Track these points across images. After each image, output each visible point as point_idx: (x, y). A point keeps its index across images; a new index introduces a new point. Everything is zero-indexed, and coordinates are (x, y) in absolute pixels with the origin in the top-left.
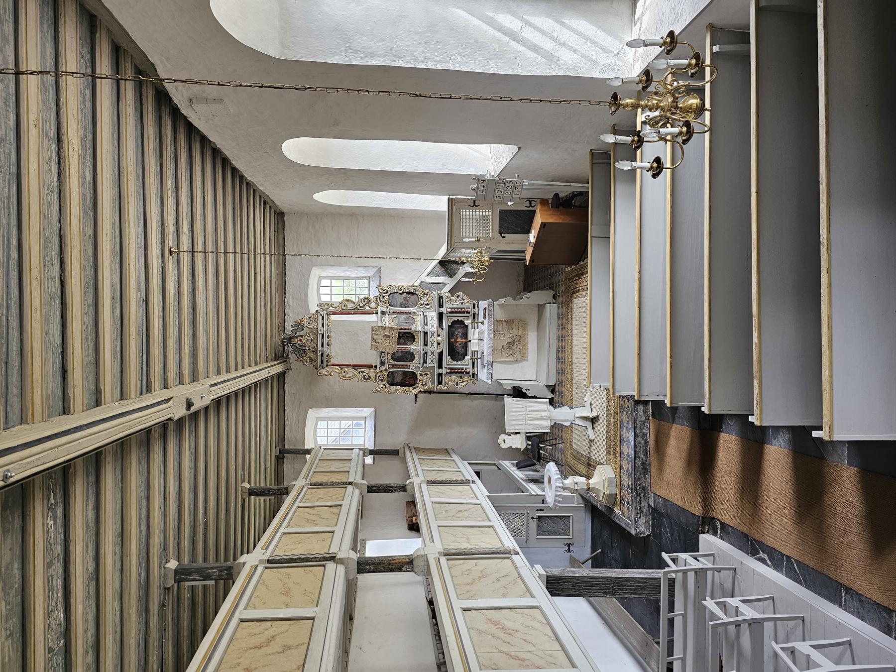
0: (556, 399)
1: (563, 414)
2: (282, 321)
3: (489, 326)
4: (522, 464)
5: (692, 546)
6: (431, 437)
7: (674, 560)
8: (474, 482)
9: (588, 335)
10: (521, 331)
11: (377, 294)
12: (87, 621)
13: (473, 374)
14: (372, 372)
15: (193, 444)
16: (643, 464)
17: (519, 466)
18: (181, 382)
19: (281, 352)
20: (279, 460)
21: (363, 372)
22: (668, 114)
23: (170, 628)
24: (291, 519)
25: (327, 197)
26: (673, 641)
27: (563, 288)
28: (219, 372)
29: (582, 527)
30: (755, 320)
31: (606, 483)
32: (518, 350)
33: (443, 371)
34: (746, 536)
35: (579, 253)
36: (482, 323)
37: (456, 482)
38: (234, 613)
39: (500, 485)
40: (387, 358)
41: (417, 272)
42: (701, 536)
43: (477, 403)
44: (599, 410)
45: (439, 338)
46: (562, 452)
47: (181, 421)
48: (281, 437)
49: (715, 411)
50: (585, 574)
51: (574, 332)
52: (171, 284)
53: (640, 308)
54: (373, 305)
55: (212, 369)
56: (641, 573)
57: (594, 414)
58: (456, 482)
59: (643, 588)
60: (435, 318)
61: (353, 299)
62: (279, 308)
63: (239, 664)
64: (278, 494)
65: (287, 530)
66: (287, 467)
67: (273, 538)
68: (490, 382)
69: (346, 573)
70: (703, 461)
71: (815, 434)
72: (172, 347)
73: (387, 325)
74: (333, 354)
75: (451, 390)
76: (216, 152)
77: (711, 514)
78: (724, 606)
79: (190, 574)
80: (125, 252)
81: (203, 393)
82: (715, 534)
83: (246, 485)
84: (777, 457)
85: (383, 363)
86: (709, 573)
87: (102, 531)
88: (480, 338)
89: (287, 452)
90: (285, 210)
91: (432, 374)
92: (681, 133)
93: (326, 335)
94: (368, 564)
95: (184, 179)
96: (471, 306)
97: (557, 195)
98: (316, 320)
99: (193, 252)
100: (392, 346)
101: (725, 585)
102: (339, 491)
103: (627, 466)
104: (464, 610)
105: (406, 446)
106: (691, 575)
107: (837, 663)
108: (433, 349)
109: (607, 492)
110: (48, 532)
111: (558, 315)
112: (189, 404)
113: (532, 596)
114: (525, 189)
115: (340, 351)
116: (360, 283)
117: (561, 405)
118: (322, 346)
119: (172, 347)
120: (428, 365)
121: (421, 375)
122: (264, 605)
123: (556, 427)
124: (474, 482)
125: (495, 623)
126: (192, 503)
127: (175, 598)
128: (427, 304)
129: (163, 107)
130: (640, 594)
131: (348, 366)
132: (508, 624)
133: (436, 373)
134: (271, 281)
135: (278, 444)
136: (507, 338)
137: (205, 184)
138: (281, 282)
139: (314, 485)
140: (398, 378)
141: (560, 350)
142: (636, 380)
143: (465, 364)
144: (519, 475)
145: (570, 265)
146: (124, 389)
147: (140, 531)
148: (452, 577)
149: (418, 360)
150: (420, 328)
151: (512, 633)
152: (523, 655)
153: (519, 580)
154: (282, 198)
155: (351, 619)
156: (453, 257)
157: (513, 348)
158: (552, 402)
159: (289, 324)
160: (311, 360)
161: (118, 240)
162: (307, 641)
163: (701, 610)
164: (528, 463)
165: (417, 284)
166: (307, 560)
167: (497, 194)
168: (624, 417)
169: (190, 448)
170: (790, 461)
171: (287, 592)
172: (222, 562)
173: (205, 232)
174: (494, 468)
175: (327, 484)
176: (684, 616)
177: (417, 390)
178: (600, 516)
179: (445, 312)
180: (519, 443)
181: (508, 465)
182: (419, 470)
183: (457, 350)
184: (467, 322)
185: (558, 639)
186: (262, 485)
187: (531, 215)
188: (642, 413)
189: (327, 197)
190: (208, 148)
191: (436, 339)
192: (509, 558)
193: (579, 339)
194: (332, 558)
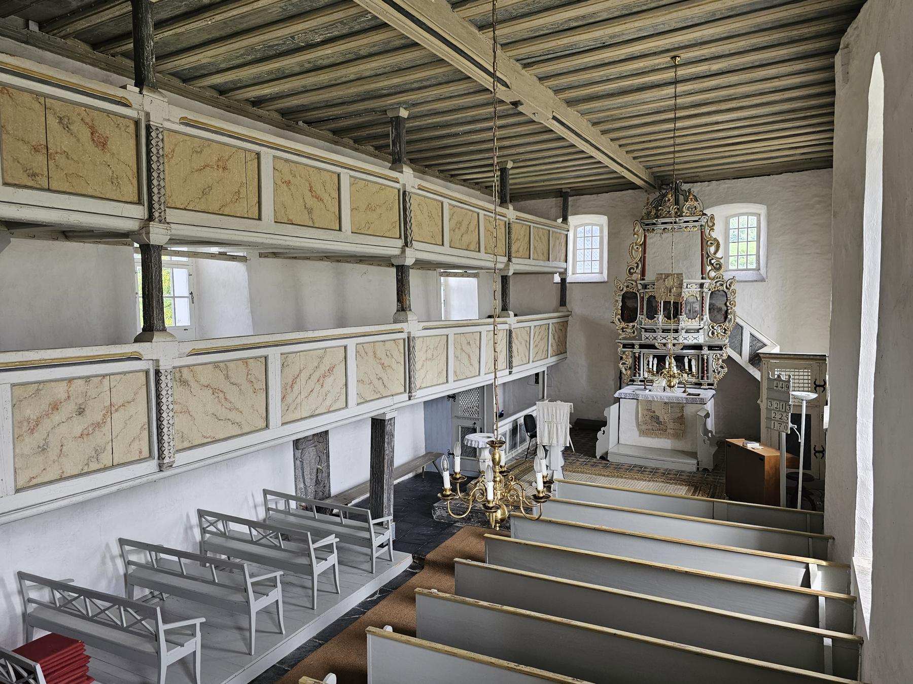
2: (702, 179)
3: (677, 398)
5: (399, 545)
10: (672, 432)
11: (726, 278)
12: (328, 58)
13: (633, 381)
21: (637, 267)
30: (498, 606)
33: (637, 350)
36: (684, 392)
53: (594, 529)
54: (713, 274)
56: (389, 500)
59: (376, 499)
60: (695, 341)
61: (719, 255)
62: (717, 174)
63: (295, 176)
69: (395, 256)
79: (396, 129)
80: (636, 17)
82: (411, 567)
83: (510, 165)
85: (645, 286)
87: (389, 55)
89: (564, 199)
93: (676, 226)
95: (774, 54)
96: (710, 381)
98: (693, 214)
108: (659, 338)
110: (362, 16)
120: (643, 334)
125: (331, 370)
128: (713, 333)
129: (845, 17)
131: (644, 251)
132: (329, 381)
138: (747, 173)
139: (509, 227)
140: (630, 304)
146: (510, 45)
147: (412, 83)
149: (647, 323)
150: (682, 324)
151: (321, 380)
152: (296, 387)
153: (379, 396)
157: (652, 421)
160: (648, 214)
161: (645, 8)
165: (738, 320)
179: (703, 352)
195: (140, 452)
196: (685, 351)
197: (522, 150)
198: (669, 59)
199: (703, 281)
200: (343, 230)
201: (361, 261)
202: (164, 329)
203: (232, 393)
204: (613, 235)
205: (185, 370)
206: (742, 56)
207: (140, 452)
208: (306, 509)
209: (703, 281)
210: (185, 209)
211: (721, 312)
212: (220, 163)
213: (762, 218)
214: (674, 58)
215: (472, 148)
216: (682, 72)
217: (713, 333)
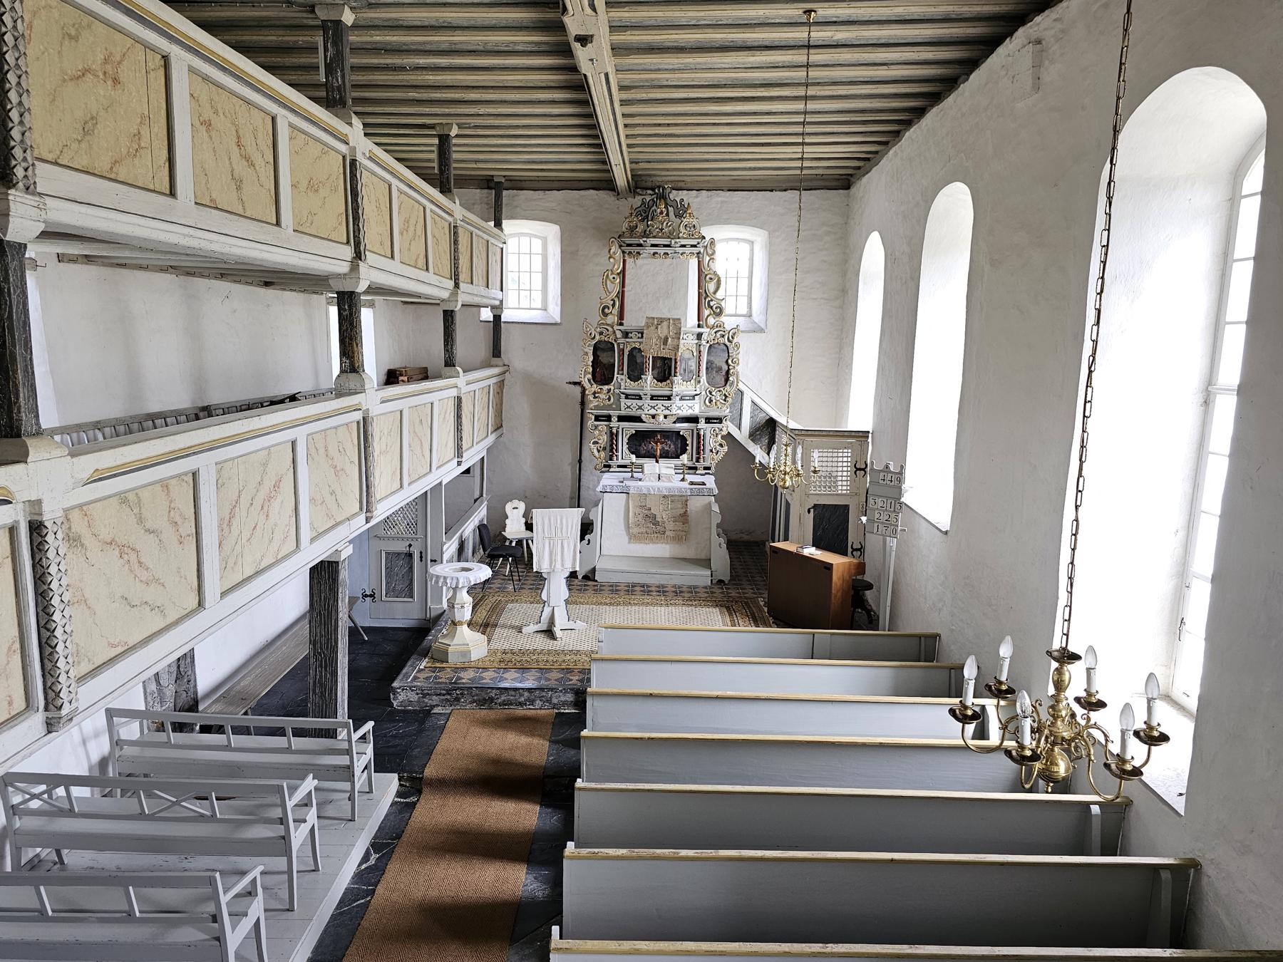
0: (576, 582)
1: (557, 590)
2: (688, 186)
3: (680, 489)
4: (484, 532)
5: (382, 763)
6: (519, 407)
7: (363, 738)
8: (459, 463)
9: (667, 625)
11: (728, 327)
13: (609, 466)
14: (612, 319)
15: (520, 48)
16: (492, 700)
17: (481, 528)
18: (613, 28)
19: (644, 184)
20: (488, 183)
21: (613, 305)
22: (1046, 732)
23: (256, 14)
24: (410, 197)
25: (873, 254)
26: (249, 734)
27: (734, 594)
28: (622, 88)
29: (400, 614)
31: (463, 648)
32: (644, 530)
33: (614, 423)
34: (399, 837)
35: (784, 616)
36: (683, 480)
37: (459, 438)
38: (285, 106)
39: (454, 501)
40: (634, 342)
41: (761, 385)
42: (396, 776)
43: (568, 472)
44: (564, 641)
45: (662, 418)
46: (502, 589)
47: (561, 28)
48: (519, 185)
49: (578, 796)
50: (340, 615)
51: (673, 609)
52: (761, 13)
53: (717, 697)
54: (711, 321)
55: (629, 78)
57: (558, 633)
58: (459, 438)
59: (322, 695)
61: (720, 295)
62: (708, 182)
63: (216, 112)
64: (443, 180)
65: (395, 194)
66: (476, 194)
67: (385, 169)
68: (599, 489)
70: (499, 780)
71: (555, 929)
72: (667, 14)
73: (682, 342)
74: (639, 262)
75: (586, 434)
76: (948, 84)
77: (426, 791)
78: (305, 804)
79: (335, 44)
81: (596, 63)
82: (399, 794)
84: (517, 880)
85: (626, 334)
86: (347, 786)
88: (661, 476)
89: (497, 193)
90: (853, 190)
91: (609, 407)
92: (1022, 747)
94: (350, 306)
95: (917, 32)
96: (707, 464)
97: (870, 586)
98: (691, 236)
99: (809, 47)
100: (652, 349)
101: (330, 806)
102: (446, 270)
103: (488, 678)
104: (294, 443)
105: (507, 369)
106: (345, 760)
107: (236, 953)
108: (646, 408)
109: (450, 649)
111: (695, 587)
112: (584, 40)
113: (313, 540)
114: (885, 542)
115: (645, 271)
116: (743, 302)
117: (570, 586)
118: (653, 245)
119: (667, 14)
121: (609, 390)
122: (295, 153)
123: (540, 579)
124: (459, 463)
126: (434, 47)
127: (297, 22)
128: (711, 401)
130: (314, 691)
132: (276, 505)
133: (611, 412)
134: (750, 169)
135: (509, 179)
136: (662, 513)
137: (904, 66)
138: (746, 185)
139: (454, 231)
140: (604, 358)
141: (646, 589)
142: (615, 690)
143: (625, 455)
144: (469, 529)
145: (768, 604)
148: (335, 428)
150: (676, 389)
152: (235, 522)
154: (875, 187)
155: (267, 284)
156: (782, 438)
157: (647, 523)
158: (573, 575)
159: (683, 195)
160: (632, 229)
162: (248, 214)
163: (299, 773)
164: (486, 541)
165: (741, 386)
166: (356, 218)
167: (879, 501)
168: (555, 675)
169: (515, 43)
170: (506, 897)
171: (313, 187)
172: (352, 94)
173: (833, 65)
174: (477, 494)
175: (456, 250)
176: (288, 750)
177: (587, 385)
178: (416, 639)
179: (700, 426)
180: (514, 529)
181: (480, 514)
182: (471, 384)
183: (644, 443)
184: (685, 458)
185: (258, 573)
186: (455, 156)
187: (841, 549)
188: (563, 699)
189: (873, 254)
190: (958, 71)
191: (661, 412)
192: (361, 509)
193: (663, 614)
194: (358, 255)
195: (10, 703)
196: (678, 425)
197: (483, 110)
198: (801, 12)
199: (700, 330)
200: (283, 225)
201: (222, 275)
202: (39, 433)
203: (147, 546)
204: (568, 256)
205: (75, 516)
206: (880, 27)
207: (10, 703)
208: (161, 728)
209: (700, 330)
210: (56, 164)
211: (723, 374)
212: (109, 68)
213: (757, 248)
214: (808, 12)
215: (413, 94)
216: (819, 35)
217: (711, 401)
